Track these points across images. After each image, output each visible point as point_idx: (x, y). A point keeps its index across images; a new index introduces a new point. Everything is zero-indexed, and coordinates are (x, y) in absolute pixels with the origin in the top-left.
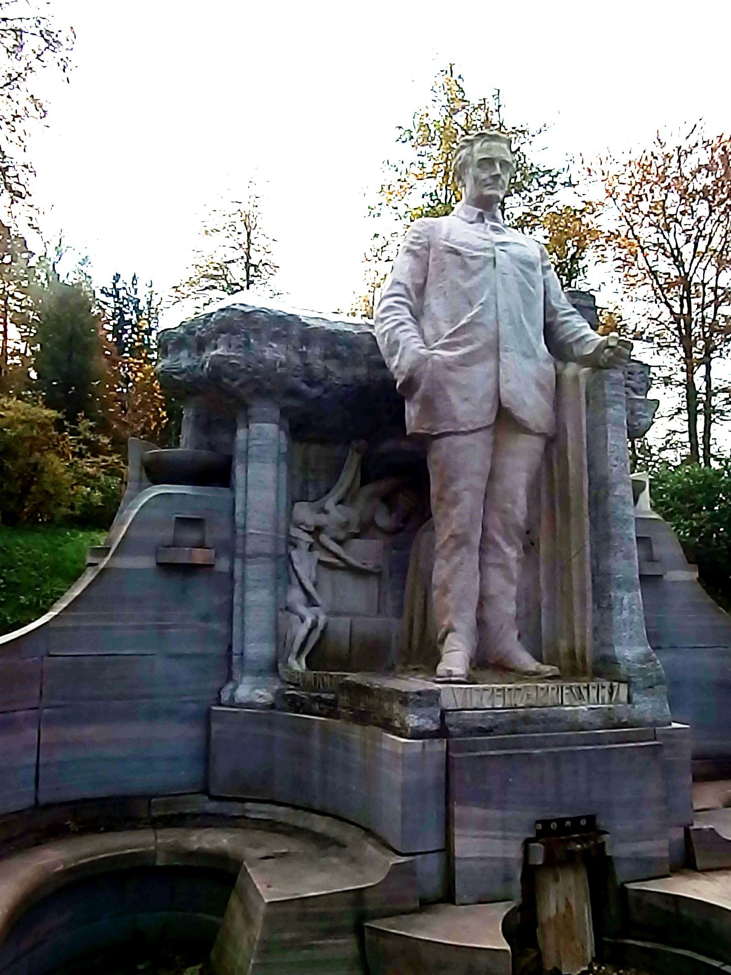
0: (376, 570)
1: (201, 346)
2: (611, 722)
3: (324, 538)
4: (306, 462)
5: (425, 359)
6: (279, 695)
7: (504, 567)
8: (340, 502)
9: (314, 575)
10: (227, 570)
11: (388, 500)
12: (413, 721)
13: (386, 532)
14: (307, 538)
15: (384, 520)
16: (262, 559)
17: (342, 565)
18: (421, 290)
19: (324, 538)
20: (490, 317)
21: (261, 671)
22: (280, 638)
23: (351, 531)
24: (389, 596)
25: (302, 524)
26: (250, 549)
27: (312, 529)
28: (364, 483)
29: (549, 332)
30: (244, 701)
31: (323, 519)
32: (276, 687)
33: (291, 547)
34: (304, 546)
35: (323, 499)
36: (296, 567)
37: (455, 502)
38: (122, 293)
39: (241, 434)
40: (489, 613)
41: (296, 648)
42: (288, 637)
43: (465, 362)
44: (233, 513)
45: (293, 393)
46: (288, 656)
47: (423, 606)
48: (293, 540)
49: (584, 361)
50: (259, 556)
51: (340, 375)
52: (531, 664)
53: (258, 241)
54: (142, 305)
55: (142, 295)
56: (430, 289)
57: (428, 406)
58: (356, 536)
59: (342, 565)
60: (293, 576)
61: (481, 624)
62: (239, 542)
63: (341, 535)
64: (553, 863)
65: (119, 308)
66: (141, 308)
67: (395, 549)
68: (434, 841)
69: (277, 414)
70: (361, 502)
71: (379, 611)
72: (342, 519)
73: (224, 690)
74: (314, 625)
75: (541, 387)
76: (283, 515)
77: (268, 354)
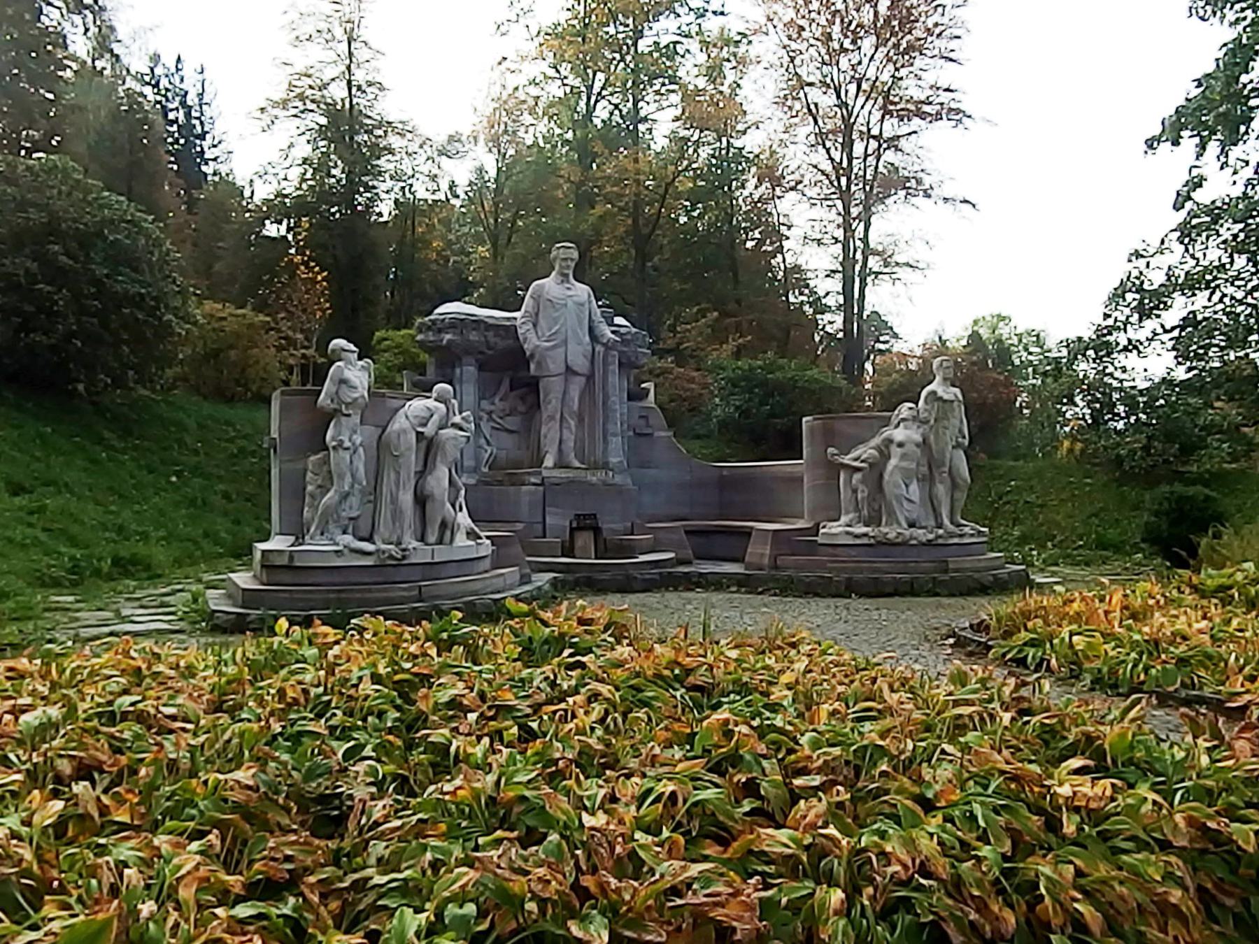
1: (440, 331)
2: (605, 484)
3: (494, 416)
5: (538, 346)
6: (479, 481)
7: (569, 428)
11: (522, 398)
12: (533, 480)
13: (521, 413)
15: (522, 408)
18: (537, 314)
20: (563, 330)
22: (477, 459)
28: (512, 390)
29: (591, 330)
31: (492, 408)
37: (550, 402)
38: (164, 83)
39: (458, 371)
40: (563, 446)
43: (554, 347)
45: (481, 353)
49: (604, 344)
51: (502, 344)
52: (577, 464)
53: (361, 53)
54: (192, 99)
55: (191, 87)
56: (541, 315)
57: (539, 364)
61: (560, 450)
64: (579, 528)
65: (160, 102)
66: (189, 103)
68: (540, 519)
75: (585, 356)
77: (471, 338)
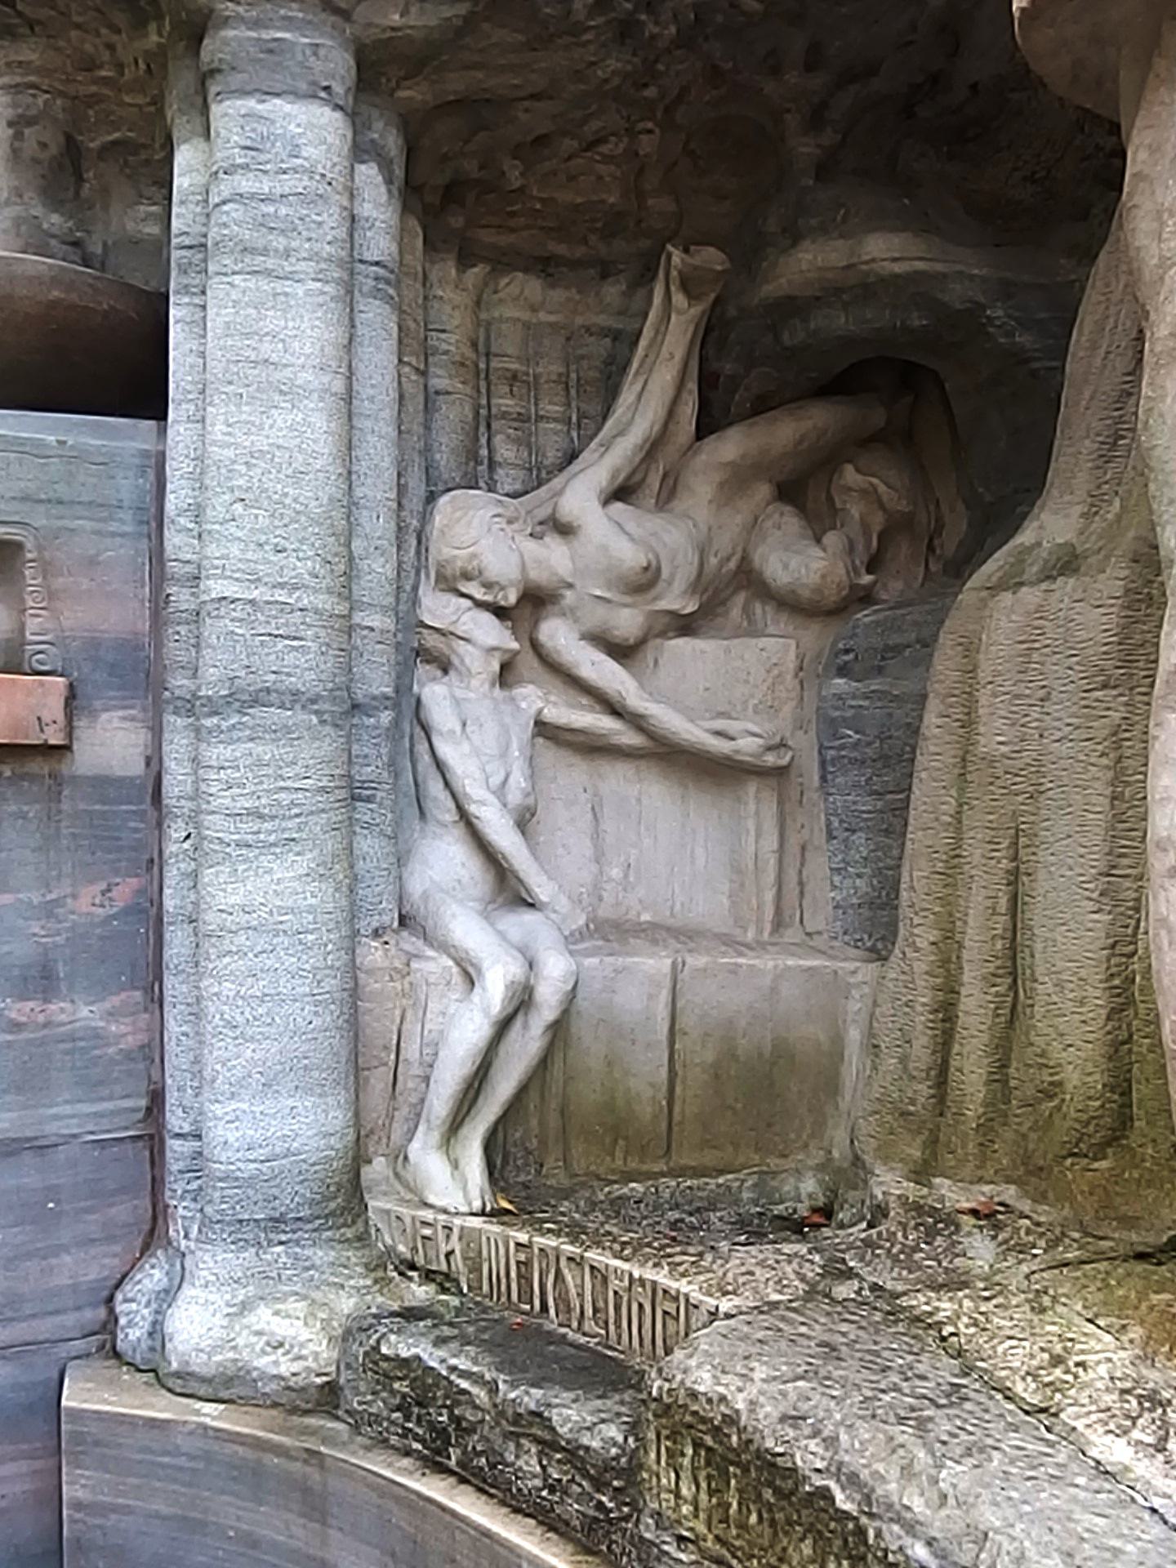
0: (770, 759)
4: (482, 346)
8: (621, 492)
9: (519, 781)
10: (137, 768)
14: (489, 632)
16: (274, 715)
17: (630, 738)
19: (558, 634)
21: (277, 1221)
23: (664, 604)
24: (819, 866)
25: (467, 576)
26: (213, 678)
27: (512, 598)
28: (706, 427)
30: (199, 1364)
32: (347, 1304)
33: (422, 670)
34: (478, 664)
35: (557, 482)
36: (444, 749)
41: (441, 1101)
42: (411, 1051)
44: (157, 520)
46: (410, 1135)
47: (1001, 923)
48: (432, 641)
50: (255, 702)
58: (685, 626)
59: (630, 738)
60: (435, 787)
62: (176, 650)
63: (627, 622)
67: (843, 671)
69: (338, 65)
70: (700, 490)
71: (778, 924)
72: (630, 556)
73: (128, 1289)
74: (522, 1001)
76: (377, 525)
